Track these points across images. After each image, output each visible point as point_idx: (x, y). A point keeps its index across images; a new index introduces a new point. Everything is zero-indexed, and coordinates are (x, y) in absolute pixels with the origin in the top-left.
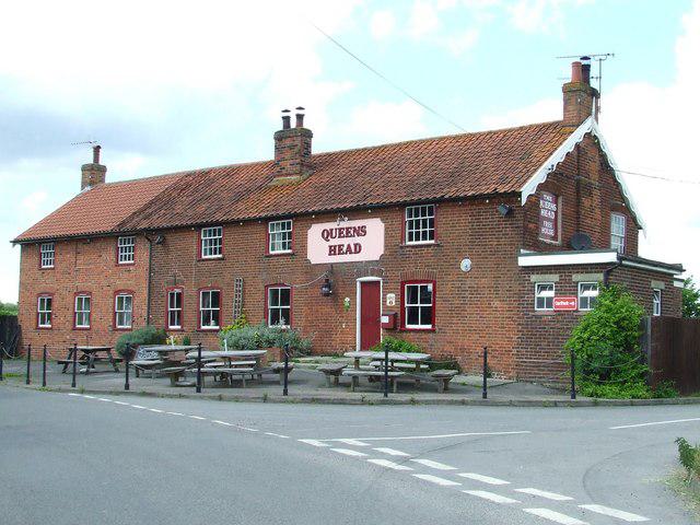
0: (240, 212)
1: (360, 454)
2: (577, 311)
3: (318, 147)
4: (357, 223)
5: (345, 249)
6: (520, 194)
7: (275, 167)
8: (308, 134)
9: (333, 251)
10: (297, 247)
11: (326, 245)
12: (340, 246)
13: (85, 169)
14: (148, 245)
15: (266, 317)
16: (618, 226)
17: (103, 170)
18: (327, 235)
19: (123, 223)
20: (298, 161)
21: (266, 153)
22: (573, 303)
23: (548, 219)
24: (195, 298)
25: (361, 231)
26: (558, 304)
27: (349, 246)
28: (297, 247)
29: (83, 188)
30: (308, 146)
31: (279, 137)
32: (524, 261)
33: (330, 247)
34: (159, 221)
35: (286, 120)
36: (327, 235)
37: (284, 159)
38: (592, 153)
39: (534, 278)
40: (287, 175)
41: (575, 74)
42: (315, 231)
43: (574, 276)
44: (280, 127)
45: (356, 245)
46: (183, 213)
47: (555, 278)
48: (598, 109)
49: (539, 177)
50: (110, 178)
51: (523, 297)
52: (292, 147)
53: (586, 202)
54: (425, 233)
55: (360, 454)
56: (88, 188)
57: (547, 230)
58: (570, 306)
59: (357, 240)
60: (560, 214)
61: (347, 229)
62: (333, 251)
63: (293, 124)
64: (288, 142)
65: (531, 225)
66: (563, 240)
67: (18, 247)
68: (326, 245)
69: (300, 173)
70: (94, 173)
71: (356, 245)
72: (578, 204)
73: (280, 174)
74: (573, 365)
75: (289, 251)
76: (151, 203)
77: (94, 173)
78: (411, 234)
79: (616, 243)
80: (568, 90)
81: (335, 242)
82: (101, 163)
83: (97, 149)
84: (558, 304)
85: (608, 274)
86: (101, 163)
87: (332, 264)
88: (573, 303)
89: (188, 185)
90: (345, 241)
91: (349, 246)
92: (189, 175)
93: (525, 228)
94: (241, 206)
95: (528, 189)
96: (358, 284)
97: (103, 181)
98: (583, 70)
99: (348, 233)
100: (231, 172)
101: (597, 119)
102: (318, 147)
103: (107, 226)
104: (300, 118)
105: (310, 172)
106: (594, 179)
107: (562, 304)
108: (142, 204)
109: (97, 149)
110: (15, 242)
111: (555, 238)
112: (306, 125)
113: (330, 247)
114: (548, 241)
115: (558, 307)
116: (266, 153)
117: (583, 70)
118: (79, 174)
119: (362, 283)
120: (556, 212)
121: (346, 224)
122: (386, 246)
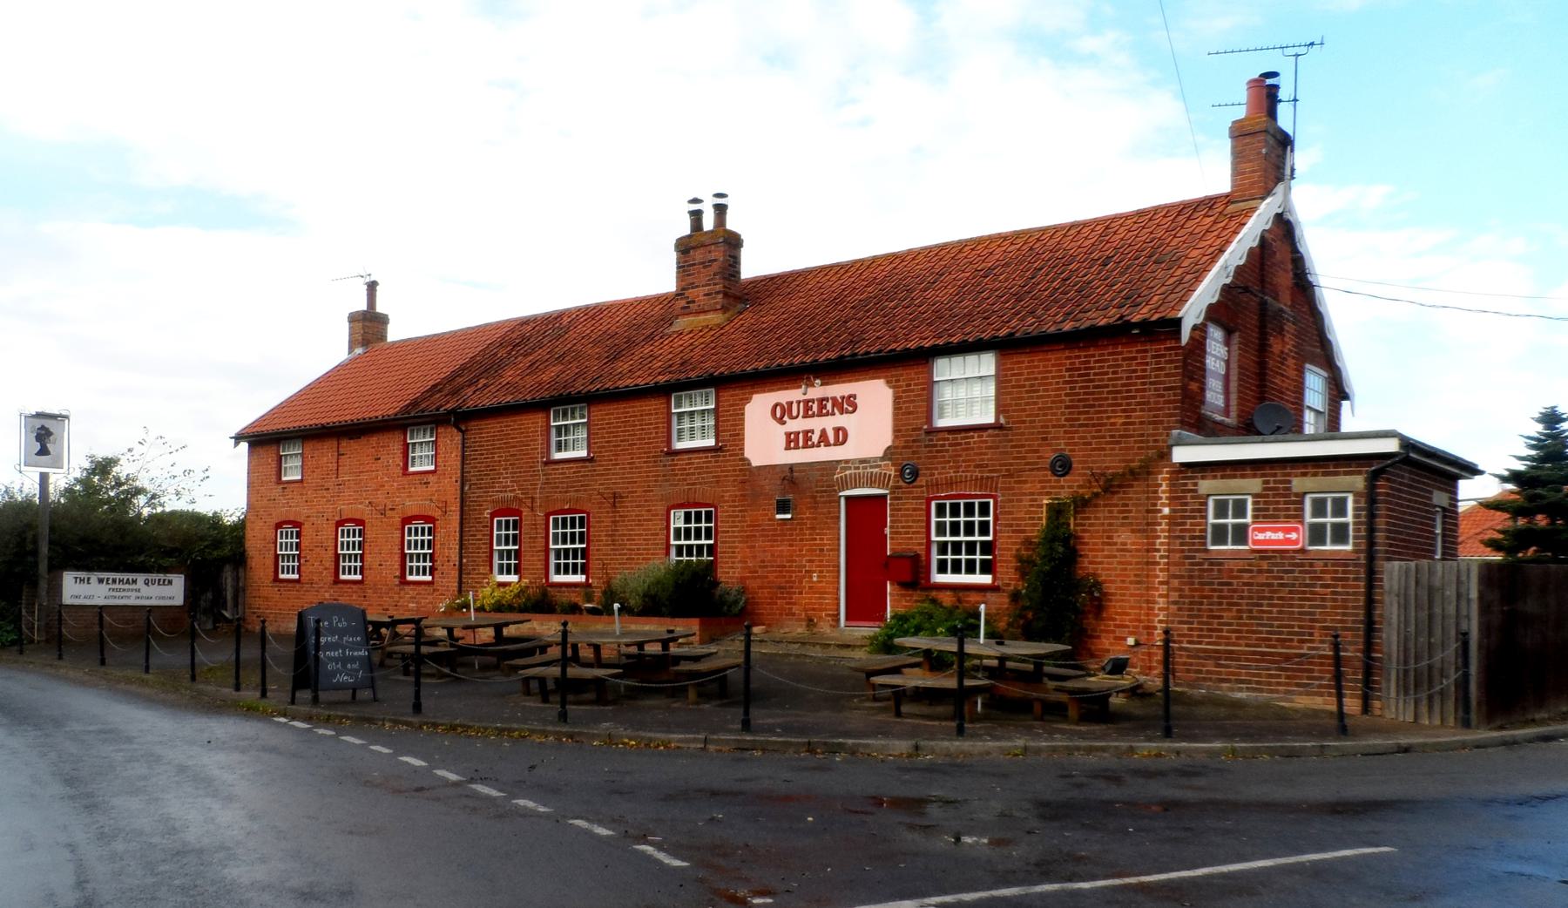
0: (622, 376)
2: (1303, 551)
3: (751, 267)
4: (838, 390)
5: (815, 438)
6: (1178, 323)
8: (733, 243)
9: (792, 441)
10: (730, 430)
11: (779, 432)
12: (806, 433)
13: (354, 318)
14: (458, 438)
19: (415, 403)
20: (718, 288)
21: (660, 278)
22: (1294, 536)
23: (1215, 374)
24: (541, 531)
25: (847, 405)
26: (1261, 536)
27: (823, 432)
28: (940, 637)
29: (351, 349)
30: (734, 263)
31: (684, 247)
32: (1181, 455)
33: (788, 435)
34: (474, 399)
35: (696, 216)
36: (781, 413)
37: (693, 286)
38: (1281, 254)
39: (1205, 485)
40: (698, 313)
41: (1253, 103)
42: (759, 406)
43: (1201, 482)
44: (685, 229)
45: (837, 430)
46: (515, 382)
47: (1255, 484)
49: (1206, 292)
50: (394, 333)
52: (706, 264)
53: (1276, 346)
54: (507, 536)
56: (359, 351)
57: (1214, 395)
58: (1288, 541)
60: (1234, 366)
62: (792, 441)
63: (708, 223)
64: (698, 256)
66: (1239, 416)
67: (244, 446)
68: (779, 432)
69: (724, 309)
71: (837, 430)
72: (1263, 348)
73: (686, 311)
74: (1338, 661)
75: (986, 579)
80: (1240, 134)
82: (380, 309)
83: (372, 287)
84: (1261, 536)
85: (1374, 477)
87: (791, 468)
88: (1294, 536)
89: (524, 339)
90: (816, 424)
91: (823, 432)
92: (525, 322)
94: (623, 366)
96: (843, 501)
97: (383, 337)
98: (1266, 93)
99: (821, 408)
102: (751, 267)
103: (387, 408)
104: (721, 210)
105: (740, 306)
106: (1284, 303)
107: (1268, 536)
109: (372, 287)
110: (238, 438)
112: (731, 225)
113: (788, 435)
115: (1256, 542)
116: (660, 278)
117: (1266, 93)
119: (848, 498)
120: (1228, 362)
121: (817, 391)
122: (897, 431)
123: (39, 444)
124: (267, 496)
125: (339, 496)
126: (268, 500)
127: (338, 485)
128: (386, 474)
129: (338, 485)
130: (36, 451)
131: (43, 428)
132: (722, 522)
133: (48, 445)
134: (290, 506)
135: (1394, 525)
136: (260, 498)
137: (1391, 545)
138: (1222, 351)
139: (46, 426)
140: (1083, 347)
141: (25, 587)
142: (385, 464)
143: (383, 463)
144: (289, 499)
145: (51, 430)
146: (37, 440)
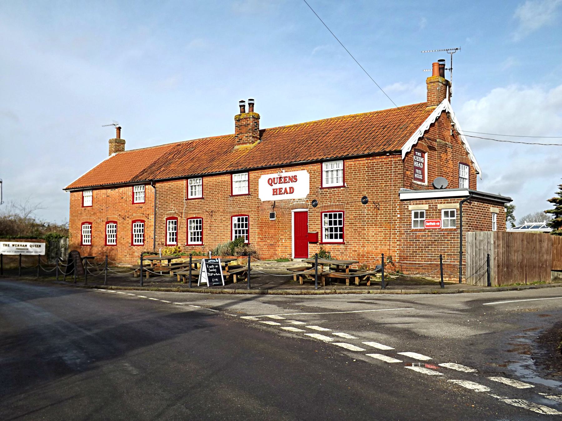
1: (300, 330)
4: (291, 174)
5: (283, 191)
7: (237, 139)
9: (275, 192)
10: (253, 187)
12: (280, 189)
15: (440, 61)
16: (464, 172)
17: (123, 142)
18: (271, 182)
21: (230, 130)
22: (438, 224)
25: (294, 179)
26: (428, 224)
27: (286, 189)
29: (110, 154)
32: (403, 196)
33: (274, 190)
45: (290, 188)
48: (450, 95)
51: (405, 219)
55: (300, 330)
59: (291, 184)
61: (285, 177)
62: (275, 192)
65: (407, 172)
70: (118, 144)
71: (290, 188)
76: (155, 163)
77: (118, 144)
78: (192, 238)
79: (466, 184)
81: (277, 186)
82: (121, 138)
84: (428, 224)
86: (121, 138)
88: (438, 224)
90: (283, 186)
91: (286, 189)
93: (404, 174)
95: (406, 148)
97: (123, 149)
100: (205, 142)
101: (449, 100)
104: (251, 105)
108: (148, 164)
111: (423, 180)
113: (274, 190)
114: (419, 183)
116: (230, 130)
118: (108, 145)
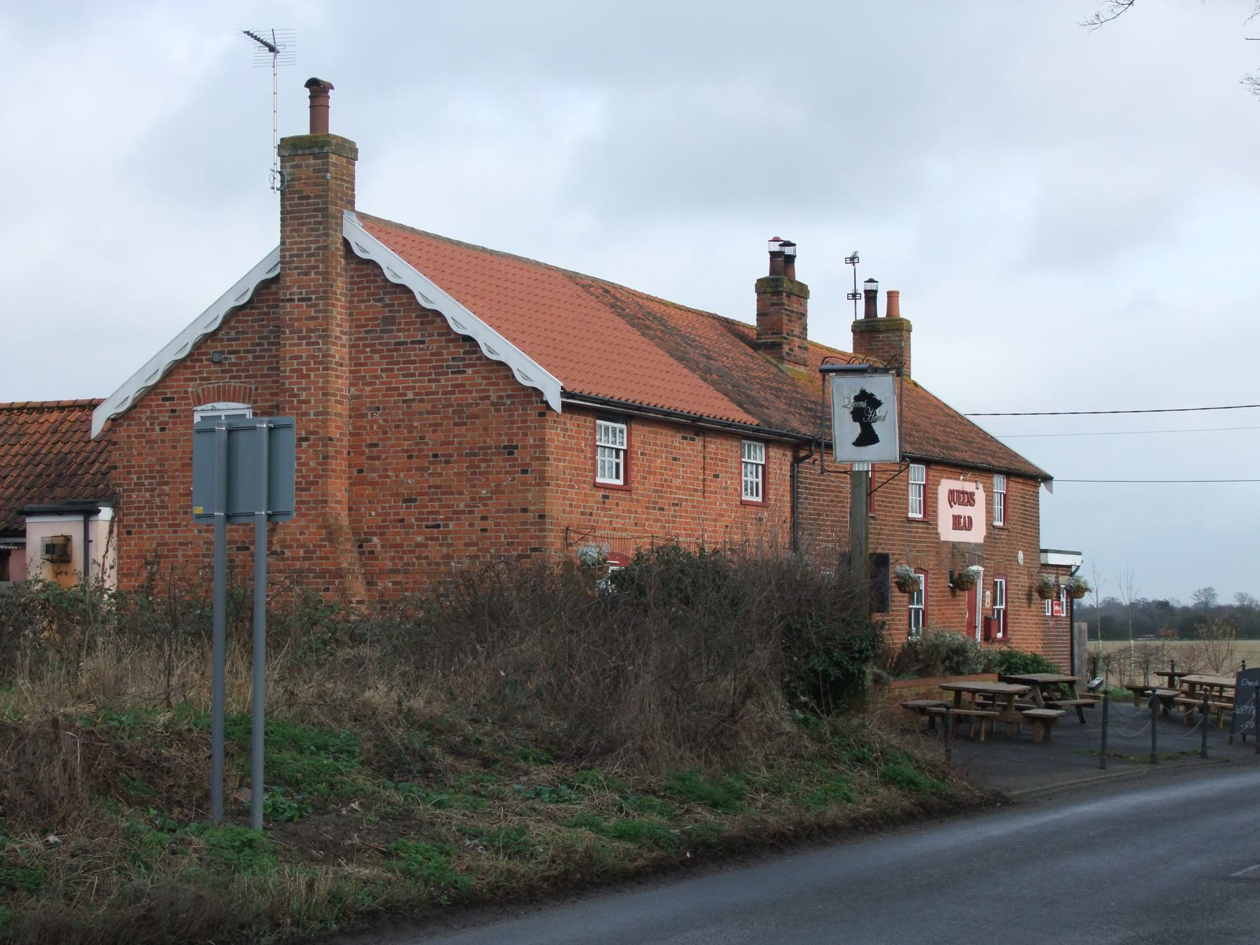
123: (858, 424)
124: (579, 507)
125: (674, 522)
126: (582, 514)
127: (673, 504)
128: (725, 498)
129: (673, 504)
130: (854, 440)
131: (863, 396)
132: (931, 587)
133: (875, 426)
134: (614, 529)
135: (1047, 644)
136: (568, 509)
137: (1044, 644)
138: (196, 927)
139: (869, 391)
140: (1001, 806)
141: (111, 582)
142: (724, 485)
143: (721, 483)
144: (612, 516)
145: (878, 398)
146: (855, 419)
